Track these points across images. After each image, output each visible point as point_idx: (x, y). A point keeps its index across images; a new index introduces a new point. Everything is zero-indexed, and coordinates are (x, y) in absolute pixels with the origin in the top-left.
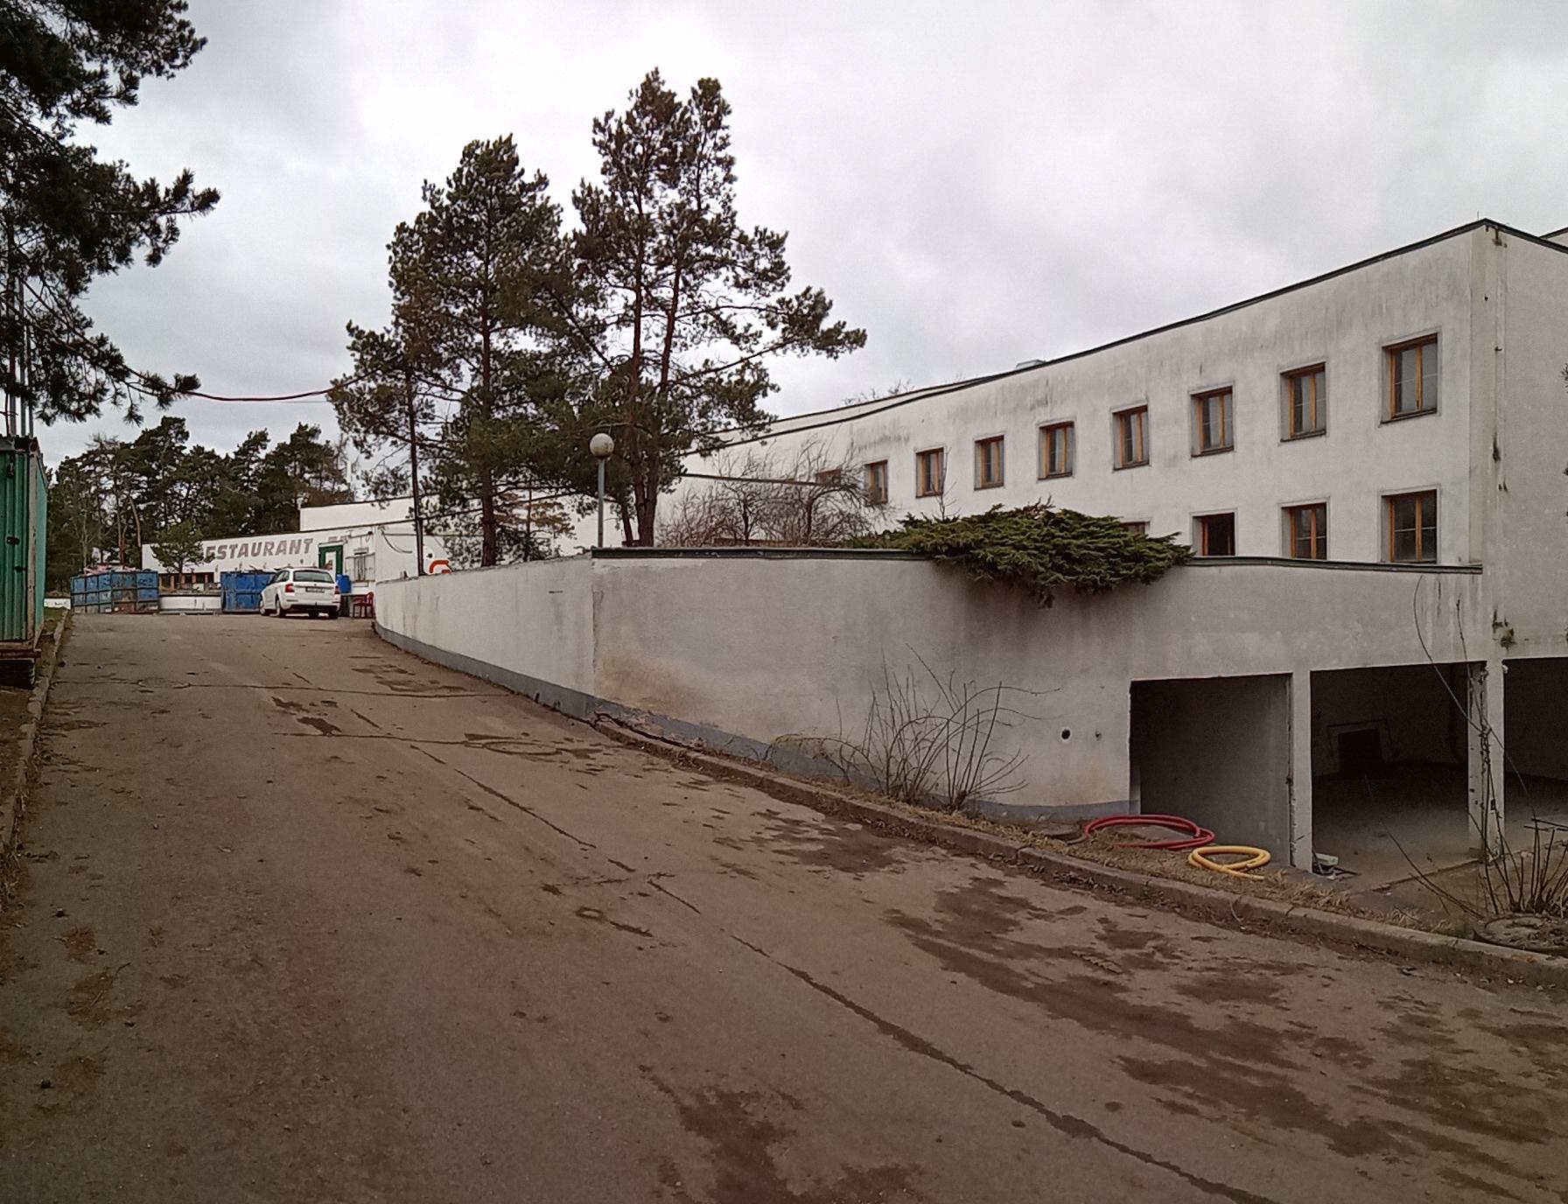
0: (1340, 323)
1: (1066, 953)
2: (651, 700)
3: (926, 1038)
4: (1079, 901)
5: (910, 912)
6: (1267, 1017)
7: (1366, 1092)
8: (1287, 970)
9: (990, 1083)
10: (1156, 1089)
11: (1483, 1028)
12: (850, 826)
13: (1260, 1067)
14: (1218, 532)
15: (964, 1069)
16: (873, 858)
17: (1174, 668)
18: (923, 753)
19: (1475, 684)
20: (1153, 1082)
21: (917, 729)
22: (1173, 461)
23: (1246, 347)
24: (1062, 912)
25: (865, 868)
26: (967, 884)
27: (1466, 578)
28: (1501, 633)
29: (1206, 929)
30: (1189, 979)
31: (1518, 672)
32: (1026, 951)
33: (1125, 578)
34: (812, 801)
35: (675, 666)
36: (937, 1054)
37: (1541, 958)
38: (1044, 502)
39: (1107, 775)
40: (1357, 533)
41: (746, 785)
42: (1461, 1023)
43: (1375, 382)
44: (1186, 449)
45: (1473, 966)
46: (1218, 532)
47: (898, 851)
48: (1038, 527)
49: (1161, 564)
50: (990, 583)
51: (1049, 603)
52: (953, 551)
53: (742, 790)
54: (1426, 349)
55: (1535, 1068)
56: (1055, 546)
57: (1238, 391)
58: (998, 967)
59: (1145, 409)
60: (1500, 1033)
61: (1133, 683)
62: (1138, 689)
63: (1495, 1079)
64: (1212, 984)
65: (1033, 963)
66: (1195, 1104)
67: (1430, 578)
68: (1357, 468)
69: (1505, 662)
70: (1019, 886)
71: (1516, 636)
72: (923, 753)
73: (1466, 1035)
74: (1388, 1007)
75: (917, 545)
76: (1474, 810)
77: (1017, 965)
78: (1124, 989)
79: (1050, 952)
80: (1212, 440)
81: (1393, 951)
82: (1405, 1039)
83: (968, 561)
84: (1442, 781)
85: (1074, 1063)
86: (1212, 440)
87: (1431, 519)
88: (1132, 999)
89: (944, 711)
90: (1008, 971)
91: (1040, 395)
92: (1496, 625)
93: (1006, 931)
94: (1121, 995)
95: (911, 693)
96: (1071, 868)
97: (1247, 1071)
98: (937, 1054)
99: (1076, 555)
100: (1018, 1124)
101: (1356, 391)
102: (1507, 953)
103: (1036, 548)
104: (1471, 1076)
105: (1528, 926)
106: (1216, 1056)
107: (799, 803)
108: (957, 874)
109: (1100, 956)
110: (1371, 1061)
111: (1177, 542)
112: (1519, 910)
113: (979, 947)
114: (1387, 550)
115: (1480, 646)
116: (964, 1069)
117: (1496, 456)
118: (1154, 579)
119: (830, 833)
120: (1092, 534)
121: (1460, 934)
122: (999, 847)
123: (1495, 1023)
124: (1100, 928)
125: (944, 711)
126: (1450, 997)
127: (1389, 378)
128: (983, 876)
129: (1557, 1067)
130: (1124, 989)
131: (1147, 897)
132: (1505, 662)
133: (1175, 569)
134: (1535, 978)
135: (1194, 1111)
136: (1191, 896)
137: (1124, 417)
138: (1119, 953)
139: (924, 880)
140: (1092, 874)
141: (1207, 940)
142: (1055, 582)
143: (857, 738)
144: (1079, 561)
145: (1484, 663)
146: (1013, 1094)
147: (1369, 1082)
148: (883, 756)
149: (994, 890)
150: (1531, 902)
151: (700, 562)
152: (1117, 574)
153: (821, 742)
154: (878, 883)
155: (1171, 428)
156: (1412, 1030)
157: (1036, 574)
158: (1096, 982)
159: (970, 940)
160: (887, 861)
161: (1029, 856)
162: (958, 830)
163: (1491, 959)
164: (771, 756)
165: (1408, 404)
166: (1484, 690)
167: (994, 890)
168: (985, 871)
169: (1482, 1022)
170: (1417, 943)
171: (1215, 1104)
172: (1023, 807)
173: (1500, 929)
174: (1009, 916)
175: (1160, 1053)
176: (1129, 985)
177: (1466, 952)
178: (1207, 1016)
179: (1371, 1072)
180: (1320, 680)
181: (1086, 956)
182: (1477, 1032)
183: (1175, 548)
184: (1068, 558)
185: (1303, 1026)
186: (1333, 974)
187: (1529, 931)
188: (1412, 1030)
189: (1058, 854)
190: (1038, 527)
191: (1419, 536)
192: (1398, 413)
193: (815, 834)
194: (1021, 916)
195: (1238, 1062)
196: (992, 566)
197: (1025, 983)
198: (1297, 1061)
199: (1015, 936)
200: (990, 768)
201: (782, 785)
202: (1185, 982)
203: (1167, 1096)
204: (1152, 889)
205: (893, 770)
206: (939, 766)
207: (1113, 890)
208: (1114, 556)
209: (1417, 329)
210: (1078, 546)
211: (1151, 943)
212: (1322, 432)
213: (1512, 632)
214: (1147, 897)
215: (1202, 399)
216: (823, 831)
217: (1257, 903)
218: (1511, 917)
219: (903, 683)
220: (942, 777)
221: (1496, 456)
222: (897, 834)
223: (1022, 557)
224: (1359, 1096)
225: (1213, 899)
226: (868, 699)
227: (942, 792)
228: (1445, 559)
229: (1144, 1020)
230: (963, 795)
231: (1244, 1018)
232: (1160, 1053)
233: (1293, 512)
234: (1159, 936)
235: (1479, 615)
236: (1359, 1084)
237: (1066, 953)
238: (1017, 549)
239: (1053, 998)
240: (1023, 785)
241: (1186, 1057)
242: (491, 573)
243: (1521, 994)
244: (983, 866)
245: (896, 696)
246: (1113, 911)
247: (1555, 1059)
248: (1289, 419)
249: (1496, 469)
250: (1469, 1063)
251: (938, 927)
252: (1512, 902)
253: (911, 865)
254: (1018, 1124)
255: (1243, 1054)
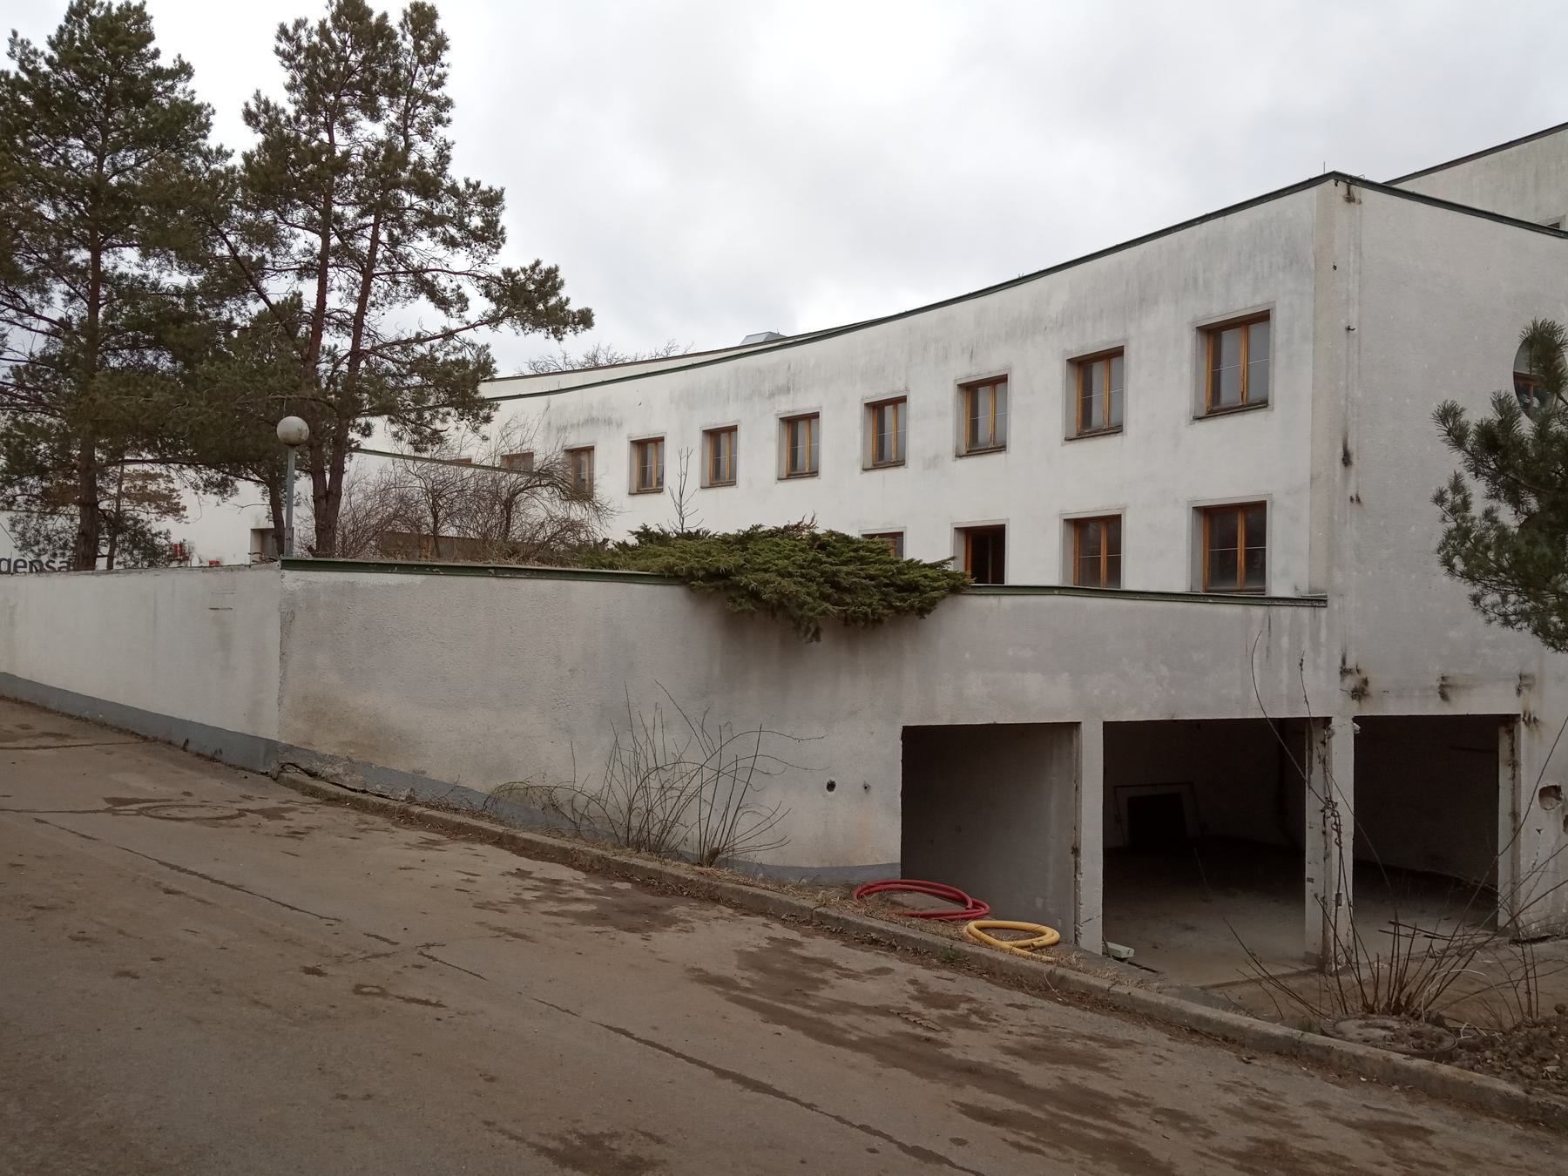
0: (1142, 300)
1: (885, 1011)
2: (350, 744)
3: (765, 1080)
4: (883, 962)
5: (714, 969)
6: (1096, 1082)
7: (1212, 1158)
8: (1113, 1044)
9: (838, 1118)
10: (1000, 1131)
11: (1334, 1119)
12: (617, 885)
13: (1100, 1123)
14: (985, 548)
15: (810, 1106)
16: (647, 920)
17: (944, 715)
18: (670, 803)
19: (1316, 744)
20: (995, 1125)
21: (664, 776)
22: (933, 462)
23: (1027, 329)
24: (869, 972)
25: (649, 927)
26: (764, 944)
27: (1305, 613)
28: (1351, 682)
29: (1019, 997)
30: (1011, 1041)
31: (1375, 735)
32: (844, 1007)
33: (898, 610)
34: (567, 858)
35: (384, 702)
36: (781, 1095)
37: (1397, 1058)
38: (807, 521)
39: (877, 834)
40: (1160, 554)
41: (482, 841)
42: (1309, 1112)
43: (1187, 370)
44: (949, 448)
45: (1321, 1061)
46: (985, 548)
47: (681, 910)
48: (802, 550)
49: (935, 594)
50: (752, 614)
51: (817, 635)
52: (714, 576)
53: (479, 847)
54: (1255, 330)
55: (1390, 1160)
56: (823, 573)
57: (1015, 383)
58: (819, 1022)
59: (903, 399)
60: (1350, 1124)
61: (905, 728)
62: (912, 736)
63: (1347, 1164)
64: (1035, 1048)
65: (851, 1019)
66: (1040, 1146)
67: (1258, 612)
68: (1162, 472)
69: (1356, 719)
70: (820, 947)
71: (1371, 688)
72: (670, 803)
73: (1313, 1122)
74: (1227, 1089)
75: (669, 568)
76: (1312, 910)
77: (838, 1020)
78: (946, 1045)
79: (867, 1010)
80: (980, 439)
81: (1228, 1038)
82: (1248, 1119)
83: (726, 588)
84: (1272, 866)
85: (915, 1105)
86: (980, 439)
87: (1257, 536)
88: (958, 1055)
89: (694, 756)
90: (829, 1025)
91: (781, 380)
92: (1344, 672)
93: (817, 988)
94: (946, 1051)
95: (658, 734)
96: (872, 929)
97: (1086, 1125)
98: (781, 1095)
99: (845, 583)
100: (873, 1151)
101: (1161, 381)
102: (1361, 1050)
103: (802, 576)
104: (1321, 1158)
105: (1384, 1028)
106: (1054, 1110)
107: (551, 861)
108: (753, 933)
109: (917, 1014)
110: (1214, 1134)
111: (950, 568)
112: (1373, 1012)
113: (794, 1003)
114: (1200, 573)
115: (1320, 695)
116: (810, 1106)
117: (1346, 460)
118: (929, 612)
119: (597, 892)
120: (862, 560)
121: (1308, 1028)
122: (790, 906)
123: (1345, 1116)
124: (911, 989)
125: (694, 756)
126: (1296, 1089)
127: (1205, 366)
128: (779, 936)
129: (1413, 1160)
130: (946, 1045)
131: (953, 960)
132: (1356, 719)
133: (950, 601)
134: (1390, 1078)
135: (1039, 1152)
136: (1000, 962)
137: (876, 409)
138: (934, 1013)
139: (720, 938)
140: (895, 935)
141: (1023, 1007)
142: (824, 613)
143: (594, 786)
144: (848, 590)
145: (1328, 720)
146: (861, 1127)
147: (1214, 1150)
148: (625, 810)
149: (794, 950)
150: (1388, 1005)
151: (418, 579)
152: (891, 606)
153: (550, 791)
154: (667, 941)
155: (932, 424)
156: (1255, 1112)
157: (801, 605)
158: (917, 1038)
159: (782, 992)
160: (670, 922)
161: (826, 916)
162: (744, 888)
163: (1341, 1055)
164: (491, 805)
165: (1228, 396)
166: (1329, 753)
167: (794, 950)
168: (779, 931)
169: (1332, 1113)
170: (1257, 1033)
171: (1060, 1149)
172: (783, 868)
173: (1350, 1027)
174: (816, 975)
175: (998, 1102)
176: (951, 1041)
177: (1313, 1046)
178: (1036, 1075)
179: (1216, 1142)
180: (1115, 733)
181: (901, 1014)
182: (1327, 1122)
183: (949, 575)
184: (836, 586)
185: (1138, 1095)
186: (1163, 1053)
187: (1384, 1033)
188: (1255, 1112)
189: (852, 913)
190: (802, 550)
191: (1241, 558)
192: (1215, 407)
193: (581, 894)
194: (829, 974)
195: (1077, 1117)
196: (754, 595)
197: (847, 1036)
198: (1137, 1123)
199: (826, 993)
200: (745, 823)
201: (525, 840)
202: (1008, 1044)
203: (1012, 1137)
204: (958, 953)
205: (635, 822)
206: (690, 817)
207: (919, 953)
208: (887, 585)
209: (1242, 303)
210: (847, 574)
211: (963, 1006)
212: (1117, 429)
213: (1366, 682)
214: (952, 961)
215: (970, 390)
216: (589, 890)
217: (1072, 975)
218: (1364, 1018)
219: (649, 722)
220: (690, 832)
221: (1346, 460)
222: (674, 893)
223: (788, 585)
224: (1205, 1160)
225: (1025, 968)
226: (606, 741)
227: (692, 849)
228: (1277, 586)
229: (974, 1072)
230: (715, 853)
231: (1075, 1081)
232: (998, 1102)
233: (1079, 527)
234: (970, 1000)
235: (1322, 660)
236: (1205, 1150)
237: (885, 1011)
238: (782, 576)
239: (884, 1050)
240: (783, 842)
241: (1024, 1108)
242: (82, 582)
243: (1375, 1093)
244: (776, 926)
245: (641, 739)
246: (922, 974)
247: (1413, 1154)
248: (1075, 414)
249: (1346, 479)
250: (1320, 1146)
251: (747, 984)
252: (1365, 1005)
253: (697, 924)
254: (873, 1151)
255: (1080, 1111)
